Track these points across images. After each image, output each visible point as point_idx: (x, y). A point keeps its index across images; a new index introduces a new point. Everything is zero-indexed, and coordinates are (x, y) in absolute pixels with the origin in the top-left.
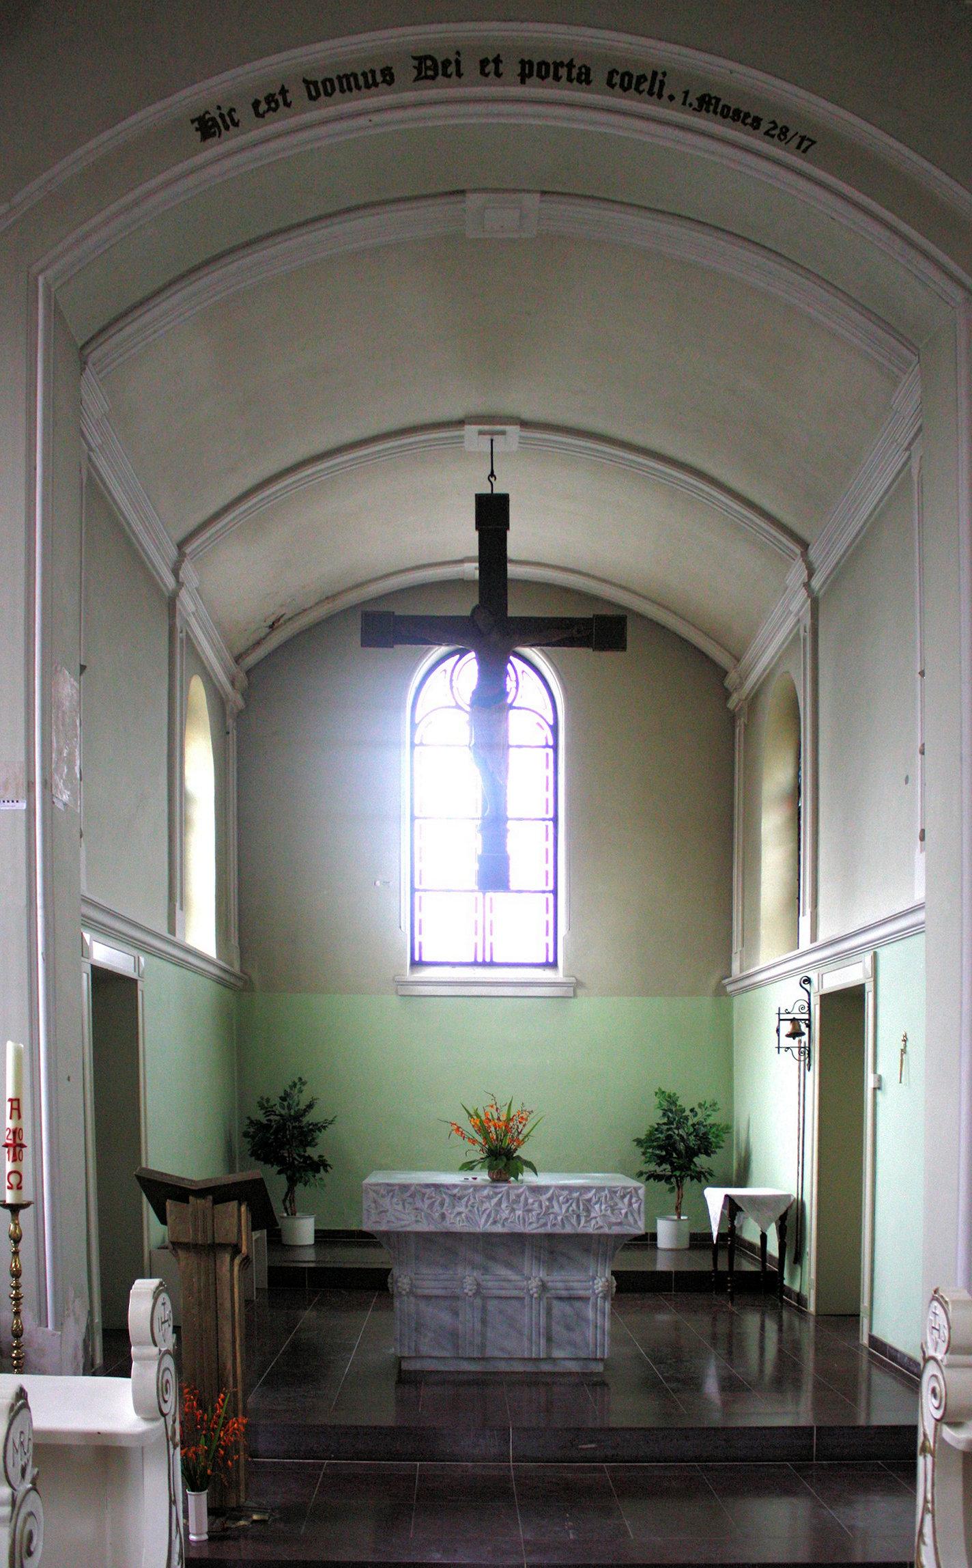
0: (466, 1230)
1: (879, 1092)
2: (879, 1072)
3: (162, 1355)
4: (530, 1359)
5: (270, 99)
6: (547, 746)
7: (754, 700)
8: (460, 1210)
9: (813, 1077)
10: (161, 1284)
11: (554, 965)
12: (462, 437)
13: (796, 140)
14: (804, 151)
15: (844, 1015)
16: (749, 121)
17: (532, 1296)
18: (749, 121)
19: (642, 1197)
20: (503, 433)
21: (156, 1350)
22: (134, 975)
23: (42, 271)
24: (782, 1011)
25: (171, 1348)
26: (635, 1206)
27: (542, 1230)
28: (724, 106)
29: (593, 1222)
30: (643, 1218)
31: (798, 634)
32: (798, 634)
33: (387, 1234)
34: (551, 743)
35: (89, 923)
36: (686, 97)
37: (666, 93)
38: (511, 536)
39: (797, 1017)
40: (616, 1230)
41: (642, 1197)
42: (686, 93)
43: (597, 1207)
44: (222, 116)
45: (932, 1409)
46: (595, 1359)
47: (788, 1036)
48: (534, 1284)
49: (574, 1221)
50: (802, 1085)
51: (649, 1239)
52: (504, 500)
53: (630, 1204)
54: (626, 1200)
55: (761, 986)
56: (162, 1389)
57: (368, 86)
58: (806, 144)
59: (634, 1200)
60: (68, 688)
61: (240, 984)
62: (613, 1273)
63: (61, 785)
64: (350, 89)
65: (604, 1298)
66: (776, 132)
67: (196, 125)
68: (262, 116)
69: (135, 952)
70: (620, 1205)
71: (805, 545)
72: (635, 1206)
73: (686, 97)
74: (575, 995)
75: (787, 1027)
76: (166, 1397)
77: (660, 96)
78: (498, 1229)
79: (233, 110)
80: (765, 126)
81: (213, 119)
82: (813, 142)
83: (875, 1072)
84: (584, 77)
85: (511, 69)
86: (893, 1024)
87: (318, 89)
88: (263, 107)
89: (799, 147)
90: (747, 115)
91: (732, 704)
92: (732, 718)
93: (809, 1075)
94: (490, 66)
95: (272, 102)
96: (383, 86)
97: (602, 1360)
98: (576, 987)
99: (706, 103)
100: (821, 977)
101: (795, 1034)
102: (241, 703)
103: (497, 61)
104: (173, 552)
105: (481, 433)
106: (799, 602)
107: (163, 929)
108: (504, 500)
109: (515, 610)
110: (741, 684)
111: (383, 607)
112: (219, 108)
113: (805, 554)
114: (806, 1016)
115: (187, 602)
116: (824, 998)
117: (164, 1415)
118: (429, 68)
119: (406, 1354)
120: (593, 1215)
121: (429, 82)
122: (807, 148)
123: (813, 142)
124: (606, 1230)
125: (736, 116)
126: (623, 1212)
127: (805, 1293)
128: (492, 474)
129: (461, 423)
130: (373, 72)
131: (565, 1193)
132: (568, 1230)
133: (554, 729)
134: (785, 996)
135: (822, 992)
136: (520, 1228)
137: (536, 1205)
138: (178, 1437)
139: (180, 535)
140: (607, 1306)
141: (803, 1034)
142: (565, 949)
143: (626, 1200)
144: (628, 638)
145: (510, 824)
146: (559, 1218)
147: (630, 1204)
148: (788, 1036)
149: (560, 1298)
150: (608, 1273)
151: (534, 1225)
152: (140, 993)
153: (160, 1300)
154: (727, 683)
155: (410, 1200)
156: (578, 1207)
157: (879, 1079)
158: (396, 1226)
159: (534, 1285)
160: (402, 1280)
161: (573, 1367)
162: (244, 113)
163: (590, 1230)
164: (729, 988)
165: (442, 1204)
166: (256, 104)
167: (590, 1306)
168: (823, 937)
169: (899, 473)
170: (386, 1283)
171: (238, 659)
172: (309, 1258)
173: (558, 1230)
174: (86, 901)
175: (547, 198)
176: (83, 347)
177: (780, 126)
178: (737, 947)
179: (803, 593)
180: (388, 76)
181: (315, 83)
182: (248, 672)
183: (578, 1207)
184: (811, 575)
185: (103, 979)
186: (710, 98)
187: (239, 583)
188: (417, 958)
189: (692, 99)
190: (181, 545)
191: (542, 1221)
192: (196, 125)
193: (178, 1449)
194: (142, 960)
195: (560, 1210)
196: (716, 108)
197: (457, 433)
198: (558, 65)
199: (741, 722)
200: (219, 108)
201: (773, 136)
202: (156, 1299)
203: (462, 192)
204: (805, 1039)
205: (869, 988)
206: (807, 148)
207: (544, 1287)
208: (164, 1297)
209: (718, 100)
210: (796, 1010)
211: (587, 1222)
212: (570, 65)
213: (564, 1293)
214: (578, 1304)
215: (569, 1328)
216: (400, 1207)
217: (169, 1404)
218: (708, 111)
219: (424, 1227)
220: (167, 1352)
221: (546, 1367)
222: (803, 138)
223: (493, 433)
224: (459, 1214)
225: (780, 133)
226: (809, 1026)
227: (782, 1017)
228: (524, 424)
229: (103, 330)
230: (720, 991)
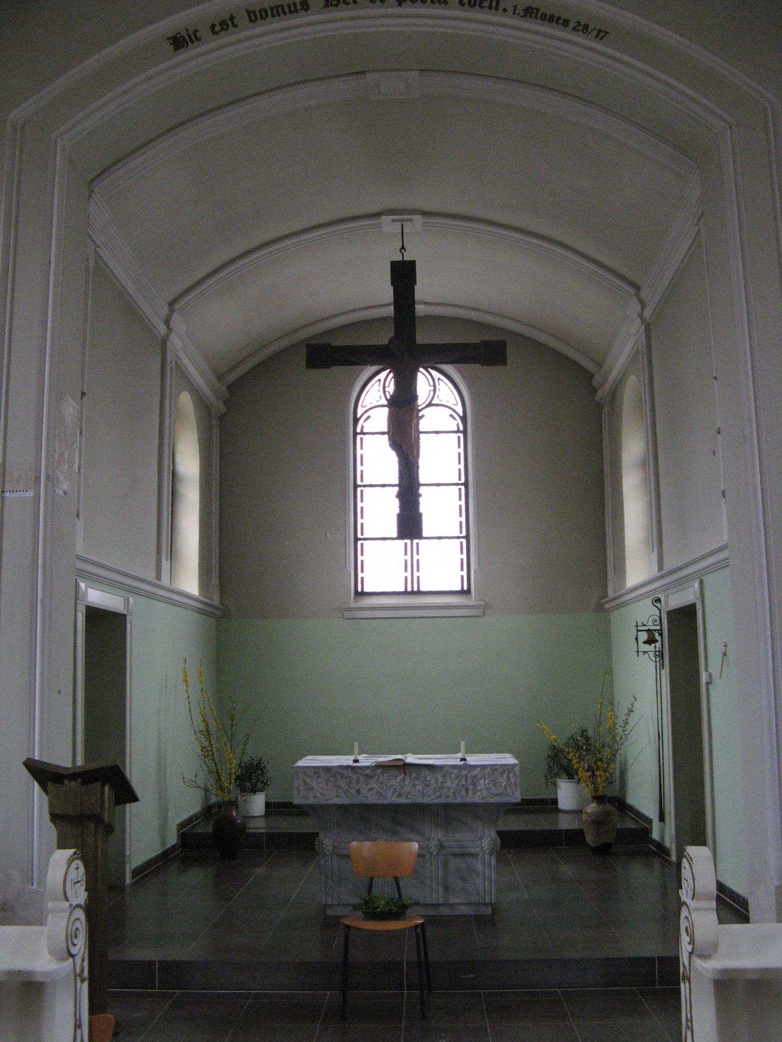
0: (375, 802)
1: (711, 687)
2: (710, 670)
3: (73, 908)
4: (432, 905)
6: (458, 431)
7: (615, 394)
8: (374, 785)
9: (665, 674)
10: (75, 853)
11: (468, 592)
12: (381, 224)
13: (595, 33)
14: (601, 39)
15: (683, 626)
16: (561, 22)
17: (431, 854)
18: (561, 22)
19: (518, 773)
20: (411, 220)
21: (67, 904)
22: (125, 612)
24: (639, 624)
25: (83, 903)
26: (513, 780)
27: (437, 801)
28: (542, 14)
29: (479, 794)
30: (519, 789)
31: (638, 350)
32: (638, 350)
33: (312, 806)
34: (461, 428)
35: (83, 574)
36: (515, 10)
37: (500, 8)
38: (418, 288)
39: (652, 628)
40: (497, 799)
41: (518, 773)
42: (515, 7)
43: (482, 781)
44: (189, 35)
45: (687, 944)
46: (485, 904)
47: (645, 643)
48: (433, 844)
49: (463, 793)
50: (658, 680)
51: (551, 805)
52: (412, 264)
53: (508, 779)
54: (505, 776)
55: (624, 606)
56: (71, 936)
57: (291, 12)
58: (602, 34)
59: (511, 775)
60: (70, 408)
61: (219, 613)
62: (499, 833)
63: (62, 477)
64: (278, 15)
65: (491, 854)
66: (581, 28)
67: (171, 41)
68: (217, 34)
69: (125, 594)
70: (501, 779)
71: (638, 288)
72: (513, 780)
73: (515, 10)
74: (484, 614)
75: (643, 636)
76: (76, 942)
77: (497, 9)
78: (403, 801)
79: (196, 31)
80: (572, 24)
81: (183, 37)
82: (607, 33)
83: (707, 670)
86: (716, 634)
88: (218, 28)
89: (597, 36)
90: (559, 18)
91: (598, 397)
92: (599, 407)
93: (663, 672)
96: (303, 12)
97: (491, 904)
98: (485, 609)
100: (667, 597)
102: (223, 409)
104: (165, 310)
105: (393, 221)
106: (635, 328)
107: (152, 577)
108: (412, 264)
109: (422, 338)
111: (325, 341)
112: (187, 30)
113: (638, 295)
114: (658, 628)
115: (176, 343)
116: (670, 613)
117: (73, 956)
119: (330, 902)
120: (479, 788)
121: (334, 8)
122: (602, 37)
123: (607, 33)
124: (491, 801)
125: (552, 19)
126: (503, 785)
127: (667, 844)
128: (403, 248)
129: (378, 215)
130: (295, 4)
131: (456, 771)
132: (459, 800)
133: (464, 419)
134: (646, 613)
135: (668, 609)
136: (420, 800)
137: (433, 780)
138: (86, 973)
139: (170, 297)
140: (493, 861)
141: (657, 641)
142: (475, 578)
143: (505, 776)
144: (508, 357)
145: (422, 490)
146: (452, 791)
147: (508, 779)
148: (645, 643)
149: (455, 855)
150: (493, 834)
151: (432, 797)
152: (128, 625)
153: (74, 865)
154: (594, 383)
155: (332, 779)
156: (467, 781)
157: (710, 675)
158: (321, 800)
159: (433, 844)
160: (327, 842)
161: (468, 911)
162: (205, 32)
163: (477, 799)
164: (607, 606)
165: (358, 782)
166: (213, 27)
167: (479, 861)
168: (667, 567)
169: (693, 243)
170: (313, 844)
171: (220, 378)
172: (259, 826)
173: (450, 801)
174: (79, 558)
175: (424, 73)
176: (91, 181)
177: (583, 23)
178: (610, 574)
179: (638, 321)
181: (254, 12)
182: (229, 387)
183: (467, 781)
184: (643, 309)
185: (95, 616)
186: (532, 9)
187: (221, 324)
188: (360, 590)
189: (520, 10)
190: (171, 304)
191: (438, 794)
192: (171, 41)
193: (86, 984)
194: (131, 599)
195: (452, 784)
196: (537, 13)
197: (377, 221)
199: (606, 410)
200: (187, 30)
201: (578, 31)
202: (69, 865)
203: (364, 72)
204: (658, 644)
205: (699, 607)
206: (602, 37)
207: (441, 846)
208: (79, 863)
209: (538, 10)
210: (650, 623)
211: (474, 793)
213: (458, 851)
214: (469, 859)
215: (463, 879)
216: (324, 785)
217: (78, 947)
218: (531, 17)
219: (343, 800)
220: (79, 906)
221: (445, 911)
222: (600, 31)
223: (402, 220)
224: (371, 789)
226: (661, 635)
227: (639, 628)
228: (424, 213)
229: (105, 170)
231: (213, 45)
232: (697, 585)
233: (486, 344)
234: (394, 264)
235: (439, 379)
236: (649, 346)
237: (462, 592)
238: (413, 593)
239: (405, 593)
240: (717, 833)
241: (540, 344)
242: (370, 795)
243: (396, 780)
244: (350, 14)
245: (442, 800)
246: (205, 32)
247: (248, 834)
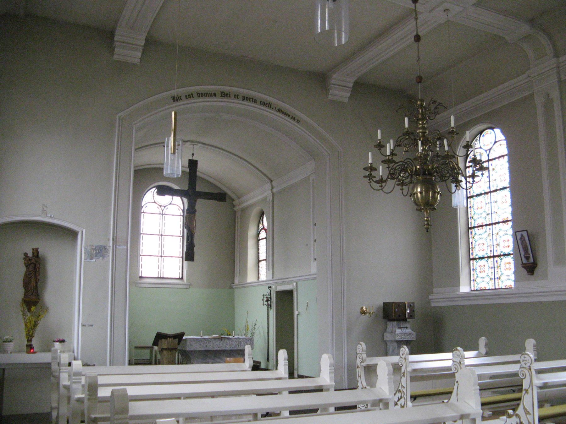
5: (189, 95)
7: (244, 210)
11: (182, 278)
23: (135, 124)
71: (272, 181)
75: (265, 299)
80: (291, 117)
84: (255, 102)
85: (241, 97)
87: (200, 95)
94: (236, 96)
95: (190, 96)
98: (189, 285)
99: (279, 110)
101: (267, 301)
103: (238, 95)
110: (240, 205)
118: (224, 94)
125: (285, 114)
128: (193, 154)
162: (183, 97)
179: (270, 192)
180: (215, 95)
184: (272, 189)
198: (250, 98)
212: (253, 99)
219: (202, 349)
225: (293, 118)
230: (231, 287)
231: (186, 102)
232: (295, 284)
233: (218, 194)
234: (190, 160)
236: (273, 201)
237: (179, 279)
238: (161, 278)
239: (158, 278)
240: (299, 359)
241: (214, 185)
242: (210, 347)
243: (218, 342)
244: (227, 100)
245: (231, 349)
246: (183, 97)
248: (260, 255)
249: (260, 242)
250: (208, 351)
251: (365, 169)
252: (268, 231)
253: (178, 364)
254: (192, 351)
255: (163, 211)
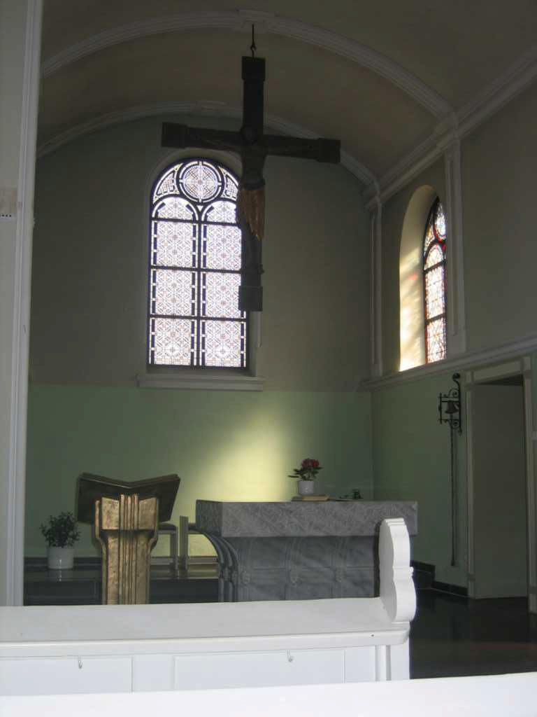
24: (442, 396)
39: (452, 399)
75: (445, 406)
108: (261, 63)
114: (457, 400)
128: (253, 46)
227: (443, 399)
234: (244, 59)
235: (227, 176)
247: (403, 517)
248: (430, 306)
249: (429, 275)
250: (284, 539)
251: (441, 423)
252: (450, 245)
253: (135, 603)
254: (236, 539)
255: (200, 214)
